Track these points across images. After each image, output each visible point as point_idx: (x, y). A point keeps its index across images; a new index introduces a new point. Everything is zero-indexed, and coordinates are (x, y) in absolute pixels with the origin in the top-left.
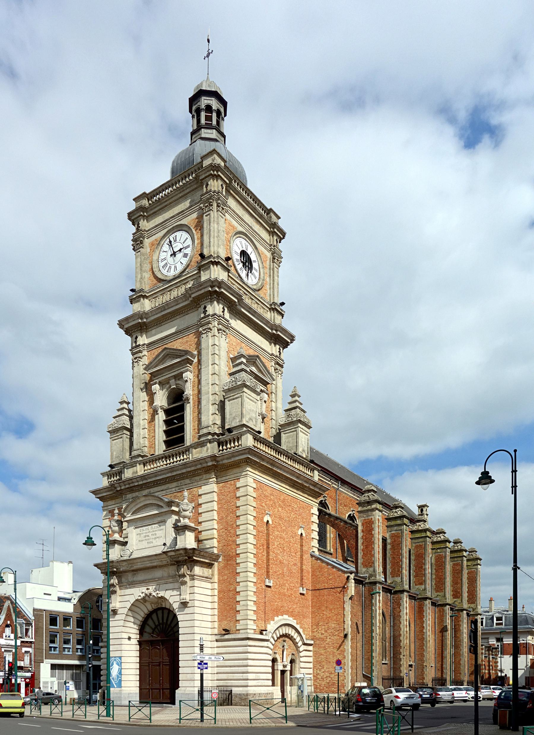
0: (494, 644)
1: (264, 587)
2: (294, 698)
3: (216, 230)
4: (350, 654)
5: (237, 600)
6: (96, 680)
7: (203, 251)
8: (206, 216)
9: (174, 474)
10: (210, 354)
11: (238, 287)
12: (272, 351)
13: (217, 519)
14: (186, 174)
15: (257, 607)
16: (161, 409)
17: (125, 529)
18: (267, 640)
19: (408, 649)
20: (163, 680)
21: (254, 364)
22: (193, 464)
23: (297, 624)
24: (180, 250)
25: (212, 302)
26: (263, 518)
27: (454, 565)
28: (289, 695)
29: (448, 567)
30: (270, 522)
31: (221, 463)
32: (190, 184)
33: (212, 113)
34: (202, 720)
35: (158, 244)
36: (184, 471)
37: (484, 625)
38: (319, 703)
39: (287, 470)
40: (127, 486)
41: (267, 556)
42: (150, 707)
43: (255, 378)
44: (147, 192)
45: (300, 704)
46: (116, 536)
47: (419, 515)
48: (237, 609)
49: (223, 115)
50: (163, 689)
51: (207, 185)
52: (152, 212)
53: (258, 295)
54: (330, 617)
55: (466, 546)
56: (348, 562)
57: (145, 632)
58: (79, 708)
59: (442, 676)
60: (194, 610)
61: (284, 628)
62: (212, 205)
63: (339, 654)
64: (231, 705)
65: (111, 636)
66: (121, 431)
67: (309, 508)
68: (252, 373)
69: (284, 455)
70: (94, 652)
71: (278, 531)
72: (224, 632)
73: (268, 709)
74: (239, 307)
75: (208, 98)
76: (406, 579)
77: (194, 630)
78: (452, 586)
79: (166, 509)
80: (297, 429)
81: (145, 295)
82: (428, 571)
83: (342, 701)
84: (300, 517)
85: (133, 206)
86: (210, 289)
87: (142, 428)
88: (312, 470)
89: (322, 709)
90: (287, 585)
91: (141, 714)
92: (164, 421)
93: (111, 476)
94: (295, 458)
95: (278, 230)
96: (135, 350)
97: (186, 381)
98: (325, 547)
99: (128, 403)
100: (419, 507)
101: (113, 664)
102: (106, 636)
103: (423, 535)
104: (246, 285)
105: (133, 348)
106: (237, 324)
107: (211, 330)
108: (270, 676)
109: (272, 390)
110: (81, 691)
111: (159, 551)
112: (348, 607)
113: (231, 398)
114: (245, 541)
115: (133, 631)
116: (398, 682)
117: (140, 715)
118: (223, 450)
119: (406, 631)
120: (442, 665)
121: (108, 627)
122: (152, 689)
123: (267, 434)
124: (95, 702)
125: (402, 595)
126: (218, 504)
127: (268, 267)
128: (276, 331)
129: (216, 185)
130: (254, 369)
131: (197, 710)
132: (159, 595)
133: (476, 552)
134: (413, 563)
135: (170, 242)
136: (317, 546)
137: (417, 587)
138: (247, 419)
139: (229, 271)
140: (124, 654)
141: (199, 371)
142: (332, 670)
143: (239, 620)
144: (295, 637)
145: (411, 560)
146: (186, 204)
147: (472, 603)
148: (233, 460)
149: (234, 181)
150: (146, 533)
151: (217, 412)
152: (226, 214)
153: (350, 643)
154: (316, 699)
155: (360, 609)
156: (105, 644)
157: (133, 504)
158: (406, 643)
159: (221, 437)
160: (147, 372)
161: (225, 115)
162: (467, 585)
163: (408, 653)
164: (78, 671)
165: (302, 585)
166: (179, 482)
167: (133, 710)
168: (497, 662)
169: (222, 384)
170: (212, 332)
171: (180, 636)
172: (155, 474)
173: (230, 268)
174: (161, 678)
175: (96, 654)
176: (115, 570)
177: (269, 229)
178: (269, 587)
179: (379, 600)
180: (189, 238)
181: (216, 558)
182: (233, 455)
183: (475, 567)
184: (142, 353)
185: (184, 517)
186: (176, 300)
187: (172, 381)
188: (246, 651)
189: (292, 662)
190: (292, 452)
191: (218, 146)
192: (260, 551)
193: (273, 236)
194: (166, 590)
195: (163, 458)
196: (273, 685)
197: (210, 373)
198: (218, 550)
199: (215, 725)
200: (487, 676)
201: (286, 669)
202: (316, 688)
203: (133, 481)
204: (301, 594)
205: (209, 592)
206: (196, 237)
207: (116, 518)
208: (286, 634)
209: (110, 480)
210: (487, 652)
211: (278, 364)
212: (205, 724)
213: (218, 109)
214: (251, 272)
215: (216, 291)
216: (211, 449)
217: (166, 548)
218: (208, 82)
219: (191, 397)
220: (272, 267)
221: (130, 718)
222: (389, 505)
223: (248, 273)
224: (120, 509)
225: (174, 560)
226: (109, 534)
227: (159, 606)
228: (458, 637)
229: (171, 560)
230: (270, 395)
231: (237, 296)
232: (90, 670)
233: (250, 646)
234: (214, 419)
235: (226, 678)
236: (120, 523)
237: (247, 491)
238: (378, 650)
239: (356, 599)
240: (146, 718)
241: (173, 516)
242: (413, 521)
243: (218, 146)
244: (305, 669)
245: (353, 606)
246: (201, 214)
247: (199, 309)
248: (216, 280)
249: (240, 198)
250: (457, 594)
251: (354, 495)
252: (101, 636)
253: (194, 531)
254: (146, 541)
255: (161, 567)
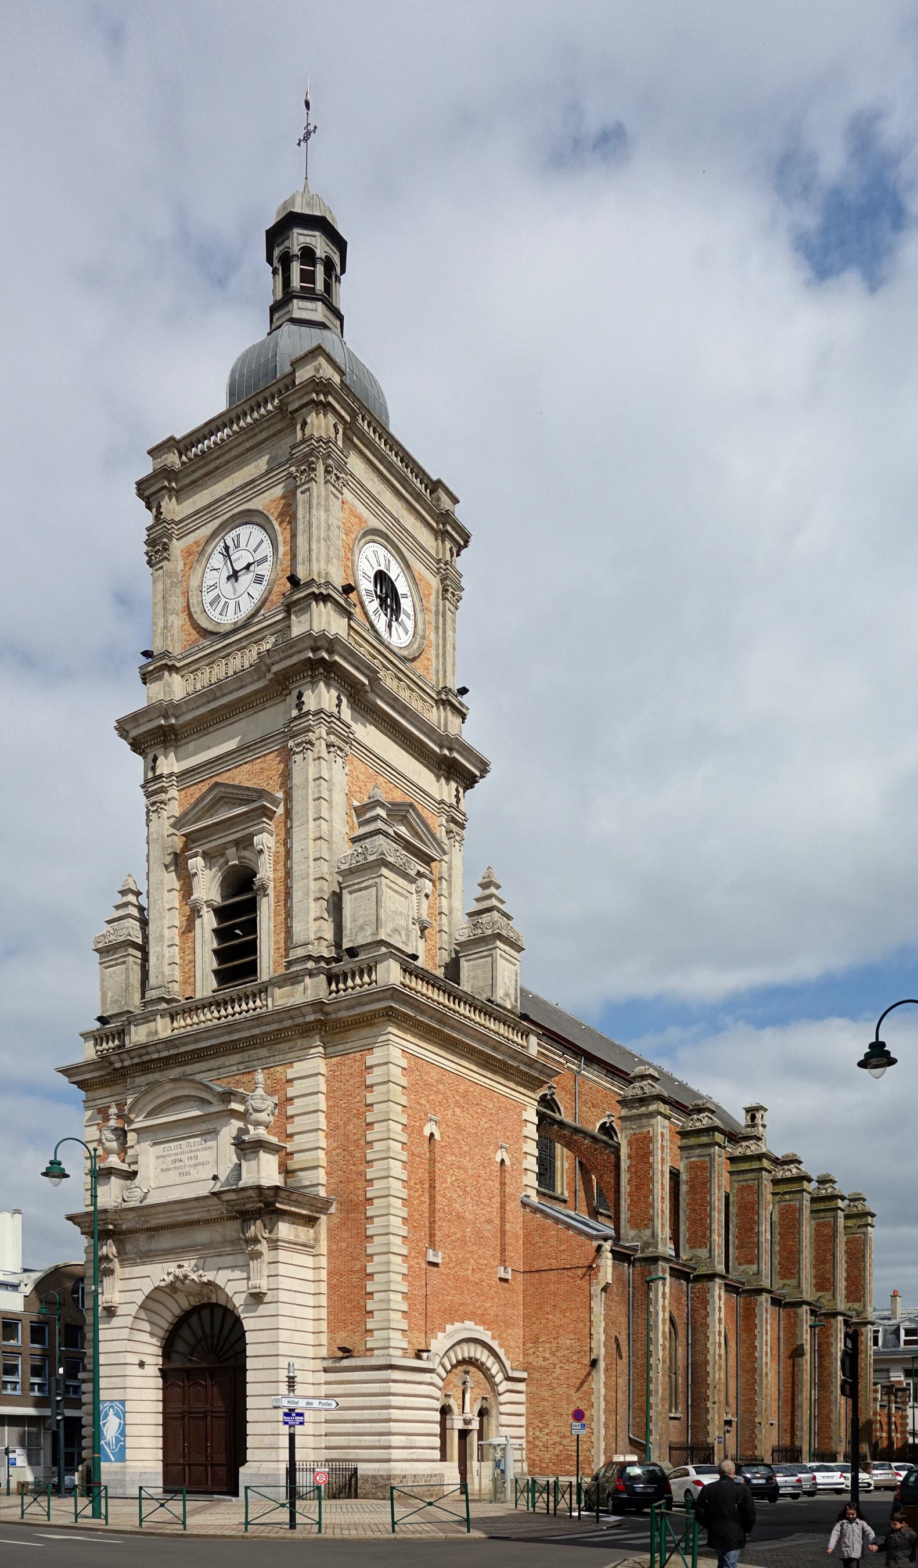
0: (900, 1382)
1: (424, 1265)
2: (487, 1484)
3: (323, 525)
4: (602, 1398)
5: (368, 1290)
6: (73, 1446)
7: (295, 570)
8: (302, 493)
9: (236, 1036)
10: (311, 798)
11: (370, 653)
12: (441, 794)
13: (325, 1128)
14: (260, 398)
15: (409, 1305)
16: (208, 906)
17: (132, 1147)
18: (431, 1371)
19: (723, 1389)
20: (212, 1446)
21: (404, 820)
22: (276, 1017)
23: (493, 1338)
24: (248, 567)
25: (314, 683)
26: (421, 1128)
27: (818, 1225)
28: (476, 1480)
29: (807, 1230)
30: (437, 1137)
31: (333, 1016)
32: (267, 420)
33: (314, 266)
34: (293, 1524)
35: (198, 554)
36: (256, 1031)
37: (880, 1344)
38: (537, 1495)
39: (472, 1032)
40: (136, 1061)
41: (430, 1205)
42: (184, 1501)
43: (405, 848)
44: (178, 437)
45: (498, 1495)
46: (114, 1161)
47: (748, 1126)
48: (368, 1309)
49: (338, 269)
50: (212, 1465)
51: (304, 424)
52: (188, 480)
53: (411, 671)
54: (561, 1326)
55: (842, 1187)
56: (600, 1218)
57: (176, 1352)
58: (35, 1499)
59: (792, 1442)
60: (277, 1308)
61: (465, 1346)
62: (314, 469)
63: (581, 1399)
64: (356, 1497)
65: (102, 1359)
66: (123, 949)
67: (518, 1110)
68: (398, 838)
69: (465, 1003)
70: (68, 1392)
71: (453, 1154)
72: (340, 1354)
73: (430, 1504)
74: (371, 696)
75: (305, 232)
76: (719, 1251)
77: (278, 1349)
78: (815, 1267)
79: (217, 1107)
80: (493, 952)
81: (174, 666)
82: (766, 1236)
83: (586, 1492)
84: (499, 1127)
85: (146, 467)
86: (311, 655)
87: (166, 943)
88: (525, 1034)
89: (544, 1505)
90: (472, 1261)
91: (166, 1514)
92: (214, 931)
93: (102, 1039)
94: (489, 1009)
95: (453, 528)
96: (153, 786)
97: (261, 852)
98: (552, 1186)
99: (138, 894)
100: (748, 1110)
101: (106, 1415)
102: (91, 1360)
103: (755, 1165)
104: (387, 647)
105: (147, 781)
106: (368, 734)
107: (313, 745)
108: (437, 1442)
109: (440, 872)
110: (40, 1469)
111: (204, 1189)
112: (598, 1306)
113: (355, 887)
114: (384, 1174)
115: (150, 1350)
116: (702, 1454)
117: (162, 1515)
118: (337, 992)
119: (720, 1355)
120: (793, 1422)
121: (96, 1342)
122: (189, 1465)
123: (431, 957)
124: (71, 1491)
125: (710, 1284)
126: (327, 1099)
127: (433, 609)
128: (450, 750)
129: (323, 425)
130: (403, 830)
131: (283, 1505)
132: (205, 1279)
133: (864, 1200)
134: (733, 1221)
135: (227, 548)
136: (536, 1184)
137: (742, 1268)
138: (389, 931)
139: (350, 616)
140: (130, 1394)
141: (288, 831)
142: (565, 1430)
143: (371, 1331)
144: (489, 1364)
145: (731, 1216)
146: (260, 465)
147: (855, 1301)
148: (358, 1011)
149: (362, 418)
150: (176, 1154)
151: (326, 916)
152: (345, 490)
153: (603, 1377)
154: (532, 1488)
155: (625, 1310)
156: (90, 1375)
157: (149, 1097)
158: (720, 1379)
159: (334, 965)
160: (177, 833)
161: (343, 271)
162: (845, 1266)
163: (723, 1398)
164: (33, 1429)
165: (503, 1262)
166: (246, 1054)
167: (148, 1507)
168: (907, 1417)
169: (335, 858)
170: (316, 750)
171: (248, 1347)
172: (196, 1036)
173: (352, 610)
174: (207, 1439)
175: (71, 1395)
176: (111, 1227)
177: (434, 525)
178: (436, 1265)
179: (664, 1293)
180: (267, 542)
181: (323, 1206)
182: (360, 1000)
183: (863, 1230)
184: (166, 792)
185: (257, 1124)
186: (240, 678)
187: (231, 852)
188: (387, 1391)
189: (483, 1413)
190: (483, 998)
191: (328, 339)
192: (417, 1194)
193: (443, 542)
194: (219, 1269)
195: (211, 1005)
196: (443, 1458)
197: (311, 836)
198: (327, 1191)
199: (319, 1535)
200: (885, 1443)
201: (470, 1427)
202: (532, 1465)
203: (149, 1049)
204: (501, 1279)
205: (310, 1275)
206: (280, 538)
207: (113, 1123)
208: (471, 1358)
209: (99, 1048)
210: (885, 1398)
211: (453, 820)
212: (298, 1534)
213: (327, 257)
214: (397, 620)
215: (323, 658)
216: (313, 989)
217: (219, 1185)
218: (306, 196)
219: (272, 885)
220: (441, 609)
221: (141, 1520)
222: (685, 1105)
223: (391, 620)
224: (120, 1106)
225: (236, 1208)
226: (95, 1156)
227: (205, 1301)
228: (826, 1368)
229: (230, 1208)
230: (437, 883)
231: (366, 671)
232: (58, 1427)
233: (394, 1381)
234: (320, 929)
235: (345, 1444)
236: (121, 1134)
237: (388, 1074)
238: (660, 1391)
239: (615, 1289)
240: (176, 1520)
241: (233, 1121)
242: (734, 1138)
243: (328, 339)
244: (510, 1427)
245: (609, 1303)
246: (292, 487)
247: (288, 698)
248: (323, 635)
249: (374, 455)
250: (824, 1282)
251: (613, 1084)
252: (83, 1359)
253: (278, 1152)
254: (176, 1170)
255: (208, 1222)
